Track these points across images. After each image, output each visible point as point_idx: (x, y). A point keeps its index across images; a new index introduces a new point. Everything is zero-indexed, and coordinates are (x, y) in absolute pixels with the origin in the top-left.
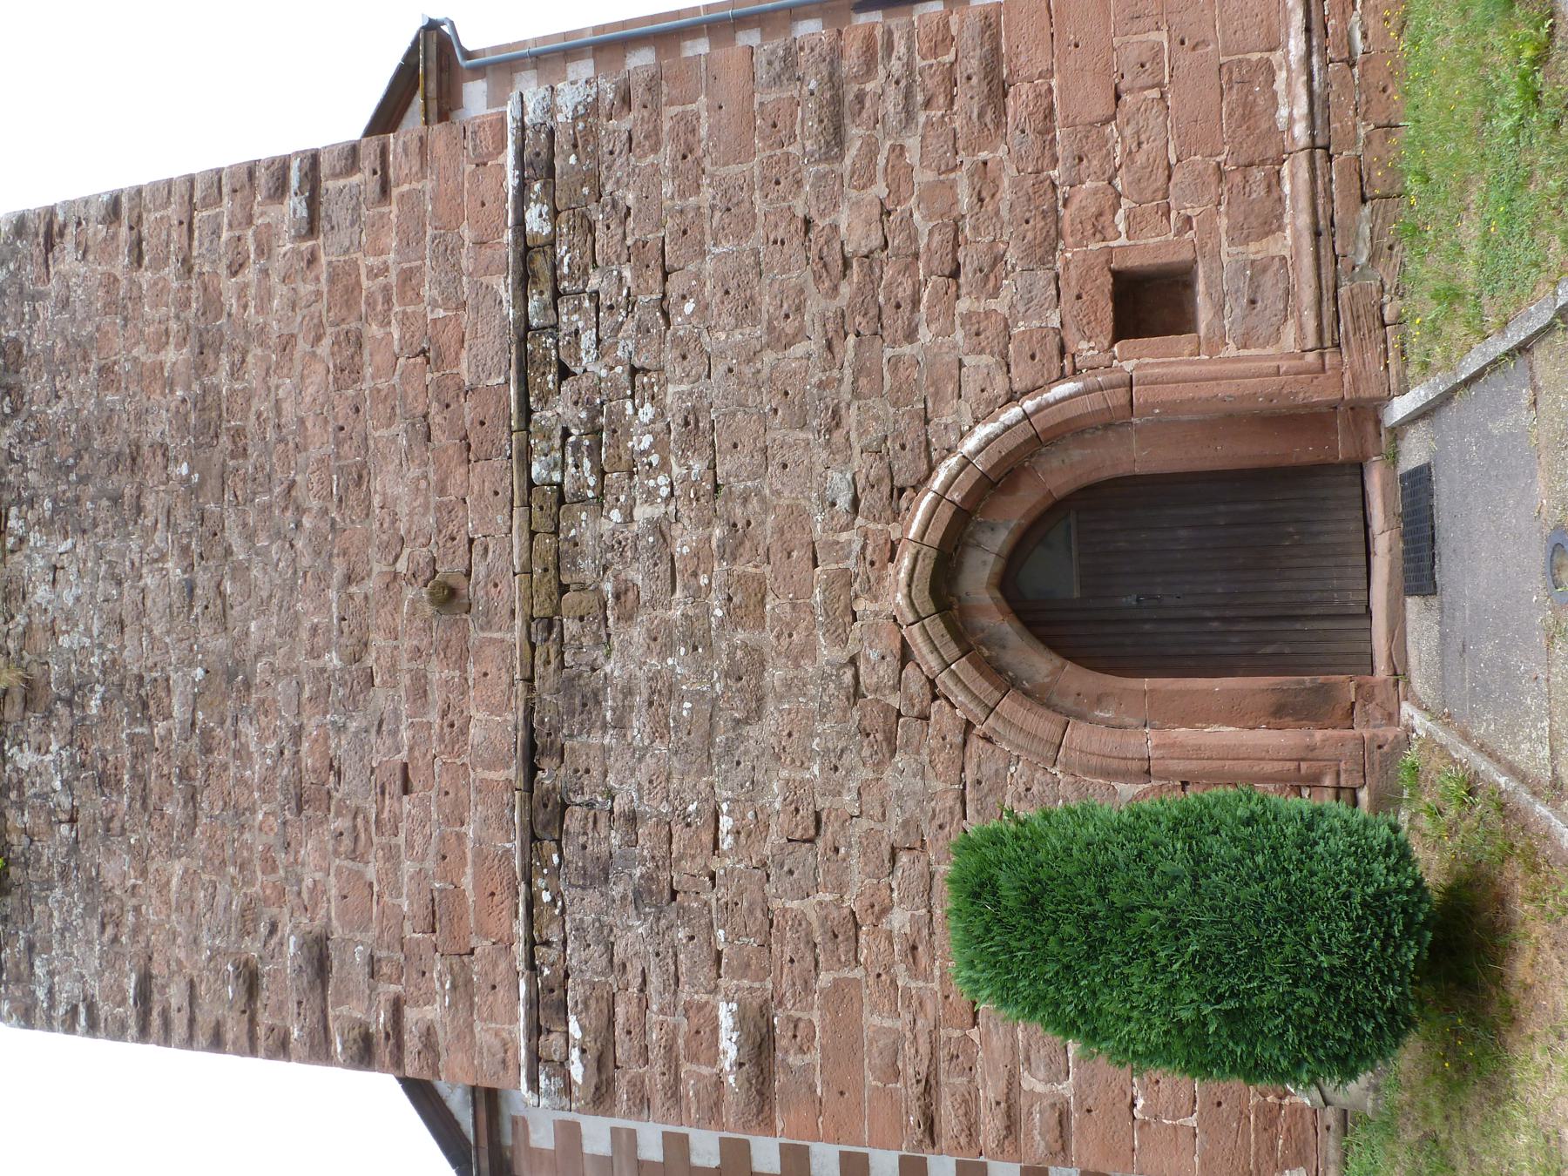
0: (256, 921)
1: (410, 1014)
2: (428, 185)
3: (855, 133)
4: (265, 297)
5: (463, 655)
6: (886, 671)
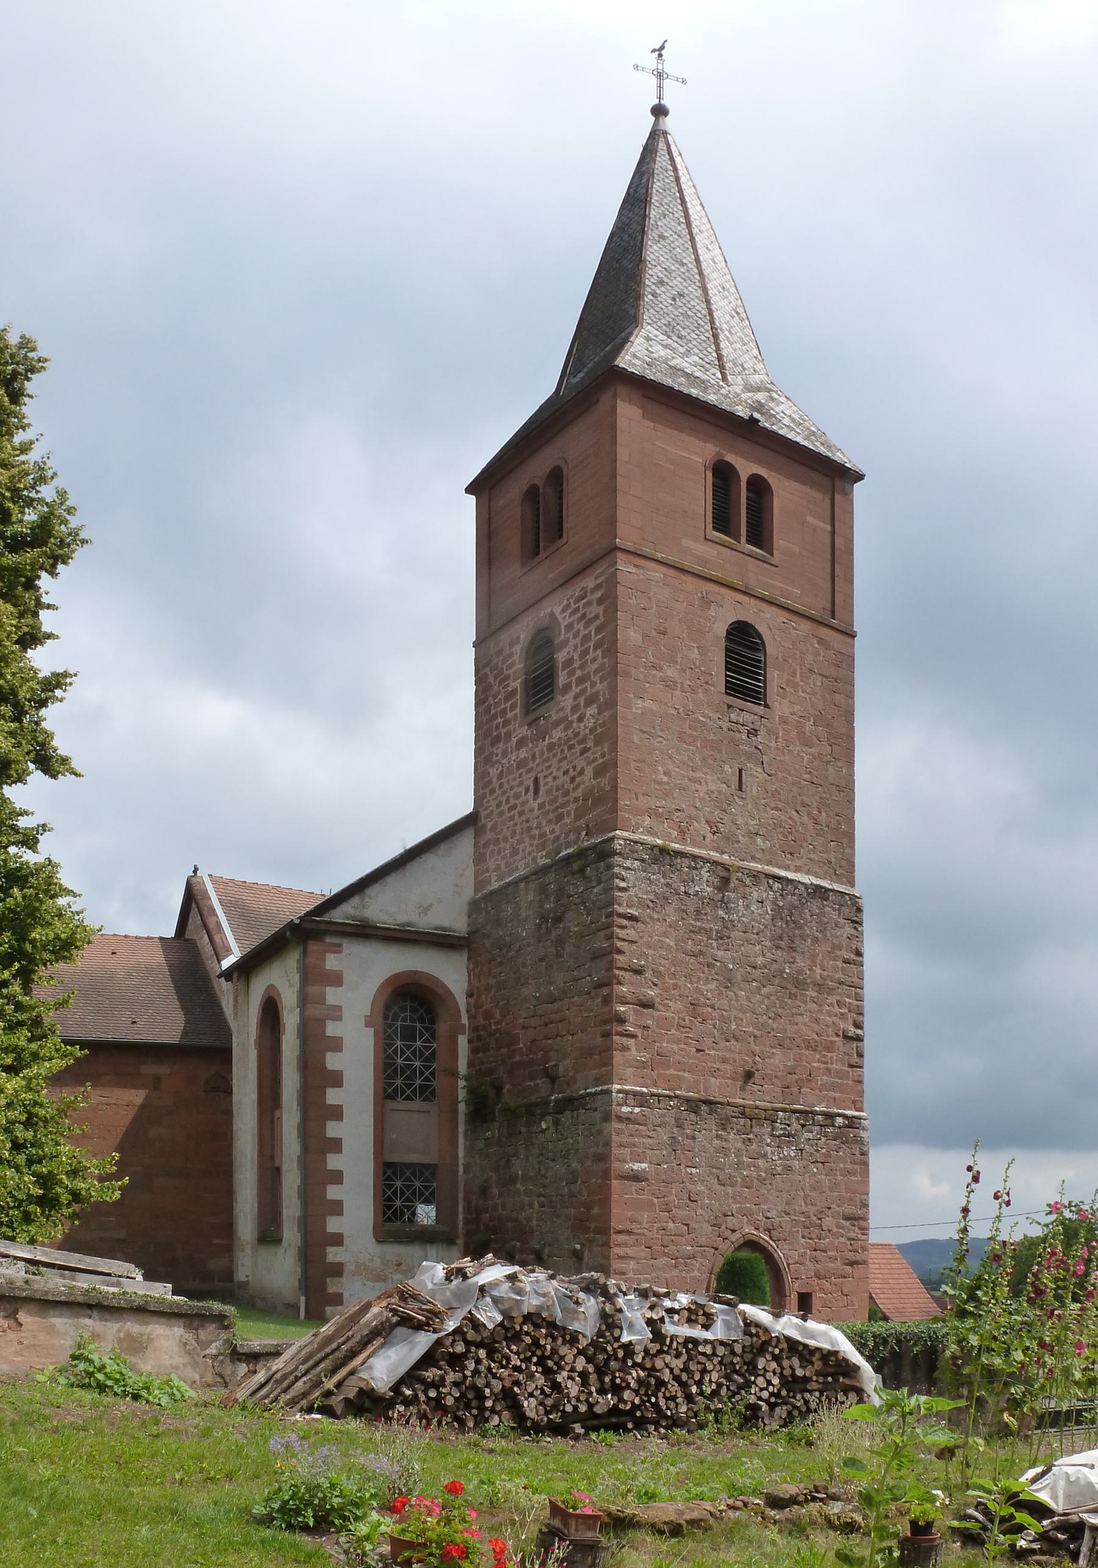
0: (657, 977)
1: (632, 1041)
2: (850, 1082)
3: (846, 1223)
4: (829, 1014)
5: (733, 1079)
6: (730, 1225)
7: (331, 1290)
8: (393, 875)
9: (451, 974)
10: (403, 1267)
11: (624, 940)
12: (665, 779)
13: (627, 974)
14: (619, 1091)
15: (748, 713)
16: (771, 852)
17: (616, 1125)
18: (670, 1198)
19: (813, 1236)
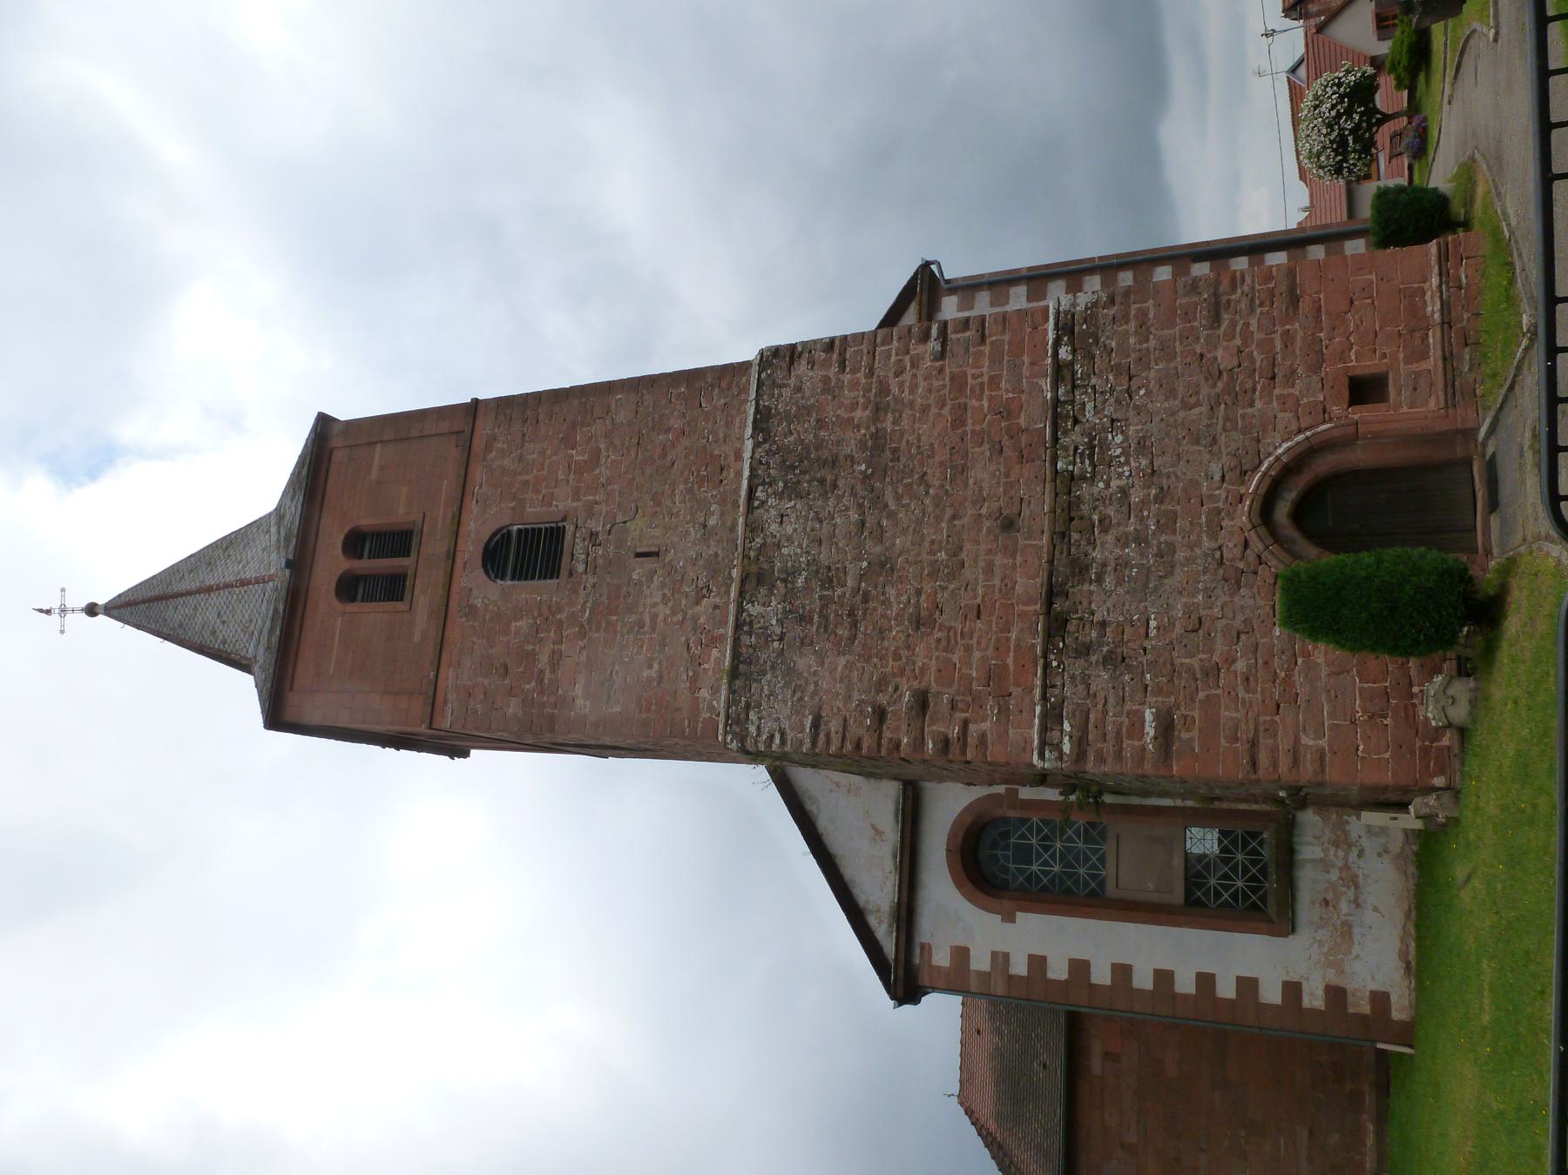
3: (1226, 317)
6: (1237, 552)
7: (1366, 1009)
8: (842, 869)
9: (949, 804)
10: (1330, 896)
11: (844, 738)
12: (656, 666)
13: (887, 734)
14: (1042, 756)
15: (576, 547)
16: (722, 502)
17: (1091, 766)
18: (1197, 667)
19: (1249, 385)
